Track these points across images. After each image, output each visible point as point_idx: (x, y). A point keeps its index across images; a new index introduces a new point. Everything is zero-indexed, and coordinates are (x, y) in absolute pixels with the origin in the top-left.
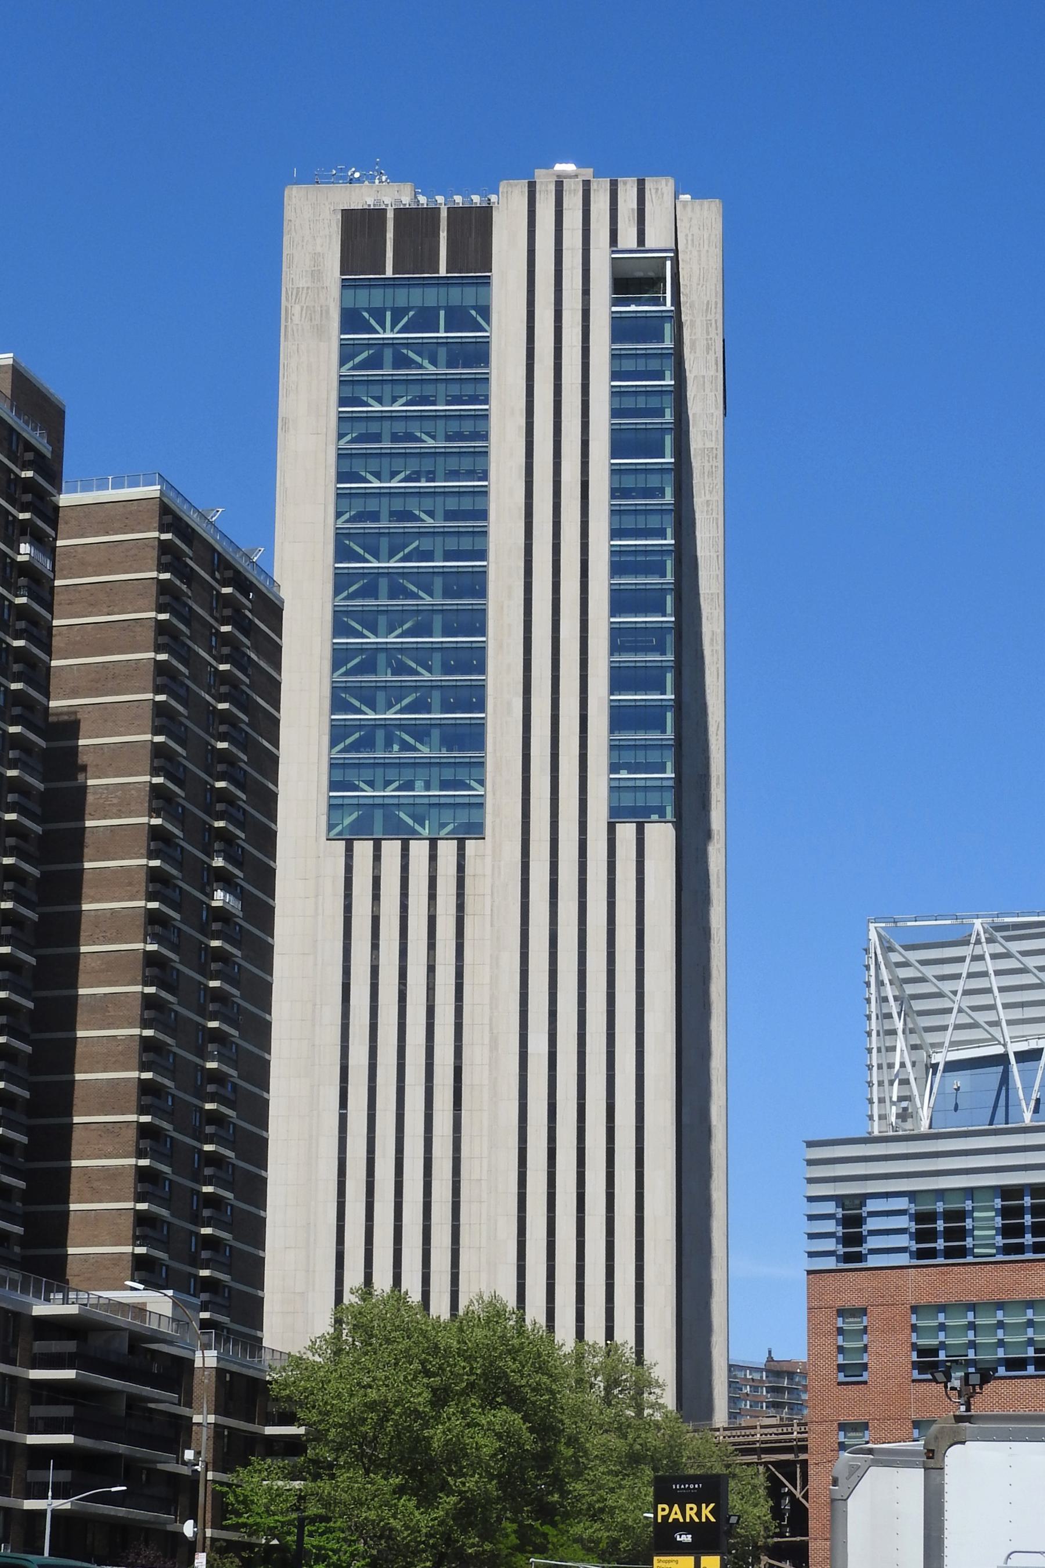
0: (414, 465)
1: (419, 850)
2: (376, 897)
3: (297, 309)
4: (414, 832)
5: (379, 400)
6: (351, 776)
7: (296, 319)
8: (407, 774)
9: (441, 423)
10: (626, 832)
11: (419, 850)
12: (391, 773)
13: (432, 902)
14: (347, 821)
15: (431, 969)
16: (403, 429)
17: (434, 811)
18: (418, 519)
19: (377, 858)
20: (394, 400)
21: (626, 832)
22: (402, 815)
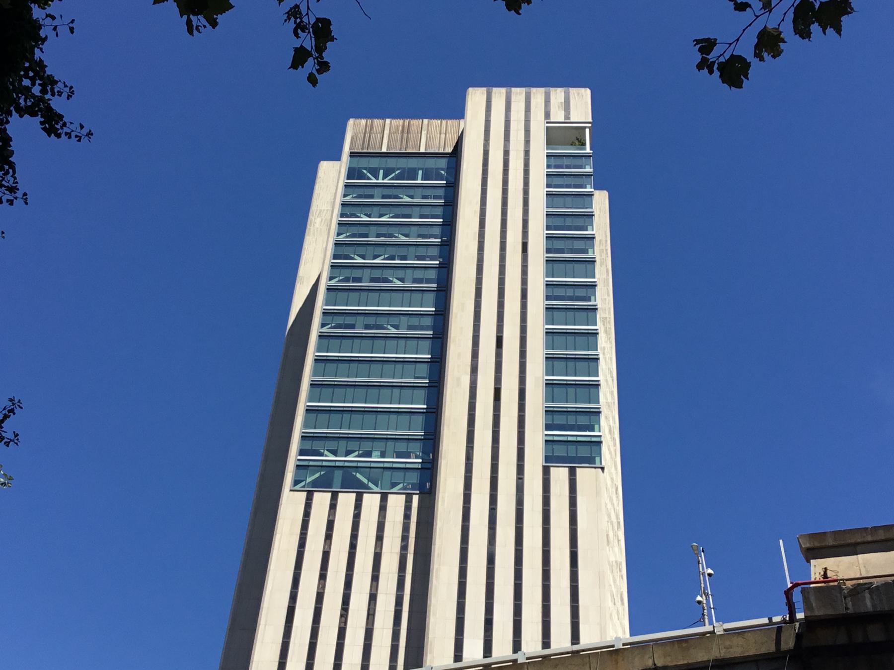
0: (391, 251)
1: (371, 501)
2: (329, 537)
3: (318, 220)
4: (366, 487)
5: (335, 453)
6: (317, 445)
7: (317, 225)
8: (367, 446)
9: (409, 271)
10: (559, 475)
11: (371, 501)
12: (352, 445)
13: (379, 543)
14: (309, 480)
15: (373, 598)
16: (379, 273)
17: (387, 474)
18: (391, 282)
19: (333, 507)
20: (348, 453)
21: (559, 475)
22: (358, 475)
